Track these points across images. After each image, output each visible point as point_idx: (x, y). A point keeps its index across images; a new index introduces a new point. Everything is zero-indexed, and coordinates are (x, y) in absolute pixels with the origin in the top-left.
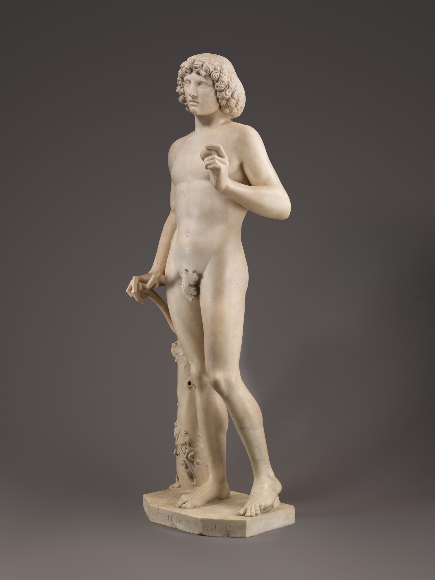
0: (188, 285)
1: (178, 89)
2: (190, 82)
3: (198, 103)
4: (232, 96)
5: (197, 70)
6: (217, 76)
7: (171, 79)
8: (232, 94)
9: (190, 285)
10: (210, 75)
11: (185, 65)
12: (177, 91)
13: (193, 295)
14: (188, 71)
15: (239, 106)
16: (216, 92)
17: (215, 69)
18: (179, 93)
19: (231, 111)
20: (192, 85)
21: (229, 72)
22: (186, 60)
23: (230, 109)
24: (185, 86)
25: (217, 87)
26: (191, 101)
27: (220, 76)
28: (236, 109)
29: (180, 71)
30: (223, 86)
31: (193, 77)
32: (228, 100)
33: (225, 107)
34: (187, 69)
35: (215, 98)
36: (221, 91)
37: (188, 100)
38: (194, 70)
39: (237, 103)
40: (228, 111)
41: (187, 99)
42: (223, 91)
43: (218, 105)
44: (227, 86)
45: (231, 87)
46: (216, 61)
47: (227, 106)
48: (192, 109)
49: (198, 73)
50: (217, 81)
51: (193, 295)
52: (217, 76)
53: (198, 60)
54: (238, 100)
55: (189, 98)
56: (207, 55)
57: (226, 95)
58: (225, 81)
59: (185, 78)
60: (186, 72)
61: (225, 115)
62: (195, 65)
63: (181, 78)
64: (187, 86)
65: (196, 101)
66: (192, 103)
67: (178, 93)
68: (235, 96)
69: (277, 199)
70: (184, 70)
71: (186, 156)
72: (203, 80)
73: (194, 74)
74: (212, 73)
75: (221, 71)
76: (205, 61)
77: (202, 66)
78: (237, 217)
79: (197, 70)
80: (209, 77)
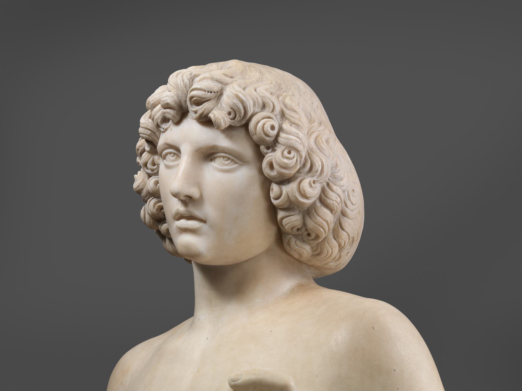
1: (140, 179)
2: (178, 150)
3: (204, 221)
4: (323, 200)
5: (201, 109)
6: (273, 128)
7: (120, 147)
8: (323, 191)
10: (246, 126)
11: (164, 94)
12: (135, 186)
14: (170, 113)
15: (344, 235)
16: (266, 183)
17: (264, 106)
19: (317, 252)
20: (185, 160)
21: (311, 121)
23: (316, 242)
24: (162, 167)
26: (179, 217)
27: (281, 129)
28: (334, 243)
29: (145, 120)
30: (292, 161)
31: (189, 134)
32: (308, 212)
33: (296, 236)
34: (167, 106)
36: (284, 181)
37: (169, 217)
38: (192, 109)
39: (340, 225)
41: (166, 210)
43: (273, 230)
44: (304, 165)
45: (318, 166)
46: (260, 80)
47: (305, 234)
48: (184, 241)
49: (206, 121)
50: (273, 145)
52: (273, 128)
53: (207, 75)
54: (343, 214)
55: (174, 206)
56: (234, 65)
58: (300, 147)
59: (161, 143)
60: (165, 120)
61: (296, 265)
62: (194, 93)
63: (148, 141)
64: (168, 167)
65: (197, 213)
66: (183, 223)
68: (333, 198)
70: (158, 112)
72: (223, 142)
75: (283, 115)
76: (228, 80)
77: (219, 95)
79: (201, 109)
80: (241, 133)
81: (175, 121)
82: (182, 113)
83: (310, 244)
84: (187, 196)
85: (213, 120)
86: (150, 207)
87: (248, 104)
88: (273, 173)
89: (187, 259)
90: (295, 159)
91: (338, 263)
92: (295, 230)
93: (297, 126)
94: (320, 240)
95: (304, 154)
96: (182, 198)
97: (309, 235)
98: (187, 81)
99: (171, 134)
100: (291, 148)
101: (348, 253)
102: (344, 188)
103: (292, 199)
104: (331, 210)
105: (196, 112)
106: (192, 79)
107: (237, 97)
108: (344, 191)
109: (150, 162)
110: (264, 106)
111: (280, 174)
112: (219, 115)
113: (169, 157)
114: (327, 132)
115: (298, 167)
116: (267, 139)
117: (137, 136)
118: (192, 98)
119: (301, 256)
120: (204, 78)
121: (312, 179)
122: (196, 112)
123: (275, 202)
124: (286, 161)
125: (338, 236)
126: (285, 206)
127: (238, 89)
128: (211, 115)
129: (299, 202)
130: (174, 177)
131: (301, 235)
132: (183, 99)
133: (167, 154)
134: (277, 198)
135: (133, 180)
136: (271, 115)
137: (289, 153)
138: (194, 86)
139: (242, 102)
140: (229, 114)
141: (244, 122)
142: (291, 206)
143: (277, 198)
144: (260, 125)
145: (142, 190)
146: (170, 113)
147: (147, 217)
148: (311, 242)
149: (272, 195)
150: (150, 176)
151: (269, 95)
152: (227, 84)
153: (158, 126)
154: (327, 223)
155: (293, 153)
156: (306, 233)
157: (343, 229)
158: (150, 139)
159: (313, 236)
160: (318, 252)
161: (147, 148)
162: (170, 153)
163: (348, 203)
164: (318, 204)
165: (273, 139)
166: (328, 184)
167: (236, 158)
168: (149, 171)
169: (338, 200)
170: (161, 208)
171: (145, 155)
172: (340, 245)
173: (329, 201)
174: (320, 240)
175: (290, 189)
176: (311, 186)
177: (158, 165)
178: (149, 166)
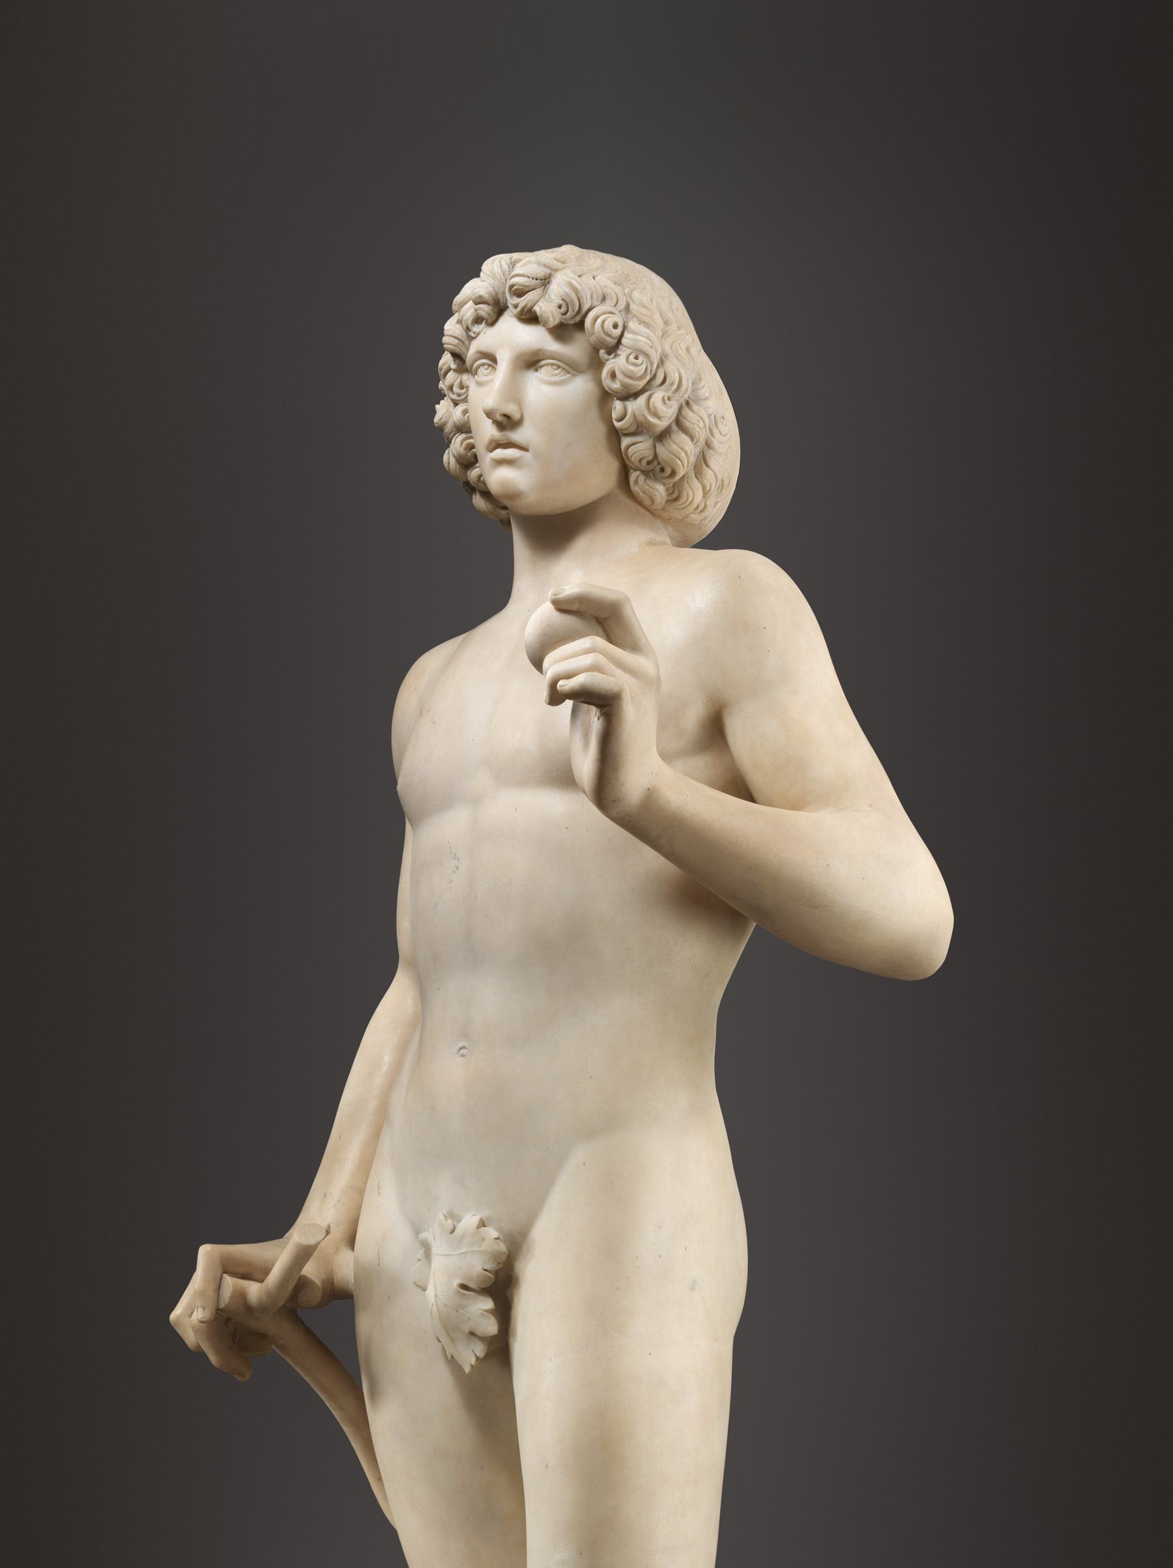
0: (456, 1282)
1: (444, 411)
3: (524, 449)
5: (523, 301)
7: (415, 364)
9: (464, 1287)
12: (436, 420)
13: (482, 1339)
15: (709, 474)
18: (448, 429)
19: (675, 495)
22: (478, 276)
25: (613, 376)
26: (496, 445)
27: (625, 328)
28: (696, 484)
29: (451, 327)
31: (511, 336)
34: (479, 301)
35: (600, 430)
36: (629, 395)
38: (512, 301)
40: (660, 491)
42: (636, 395)
45: (674, 377)
47: (656, 469)
48: (499, 478)
49: (530, 317)
50: (613, 349)
51: (482, 1339)
52: (615, 326)
54: (708, 445)
56: (568, 251)
57: (656, 415)
58: (647, 349)
64: (479, 384)
66: (500, 453)
67: (441, 428)
69: (893, 887)
71: (473, 715)
72: (552, 345)
73: (509, 324)
74: (591, 315)
75: (627, 308)
78: (704, 964)
79: (523, 301)
81: (490, 321)
82: (499, 309)
83: (664, 484)
84: (505, 415)
85: (539, 314)
86: (458, 444)
87: (583, 294)
88: (616, 386)
89: (503, 509)
90: (644, 366)
91: (703, 515)
92: (644, 462)
93: (647, 325)
94: (677, 478)
95: (702, 443)
96: (499, 418)
97: (662, 470)
98: (505, 266)
99: (487, 338)
100: (638, 353)
101: (716, 503)
102: (710, 411)
103: (640, 418)
104: (692, 439)
105: (516, 307)
106: (513, 264)
107: (570, 285)
108: (709, 416)
109: (456, 383)
110: (604, 299)
111: (624, 386)
112: (547, 307)
113: (482, 370)
114: (688, 338)
115: (648, 378)
116: (608, 339)
117: (441, 350)
118: (511, 287)
119: (653, 502)
120: (529, 262)
121: (667, 395)
122: (516, 307)
123: (617, 425)
124: (631, 367)
125: (701, 475)
126: (632, 430)
127: (571, 275)
128: (537, 308)
129: (649, 422)
130: (486, 392)
131: (653, 470)
132: (501, 290)
133: (479, 367)
134: (620, 420)
135: (435, 412)
136: (614, 310)
137: (636, 358)
138: (515, 272)
139: (576, 291)
140: (560, 307)
141: (578, 319)
142: (640, 428)
143: (620, 420)
144: (599, 321)
145: (445, 424)
146: (484, 310)
147: (452, 460)
148: (666, 481)
149: (614, 416)
150: (456, 404)
151: (612, 285)
152: (556, 270)
153: (468, 329)
154: (686, 453)
155: (641, 358)
156: (658, 468)
157: (707, 466)
158: (458, 351)
159: (668, 471)
160: (675, 495)
161: (453, 366)
162: (483, 365)
163: (715, 431)
164: (674, 427)
165: (615, 341)
166: (687, 403)
167: (571, 368)
168: (454, 397)
169: (701, 424)
170: (471, 447)
171: (451, 376)
172: (704, 488)
173: (688, 424)
174: (677, 478)
175: (636, 406)
176: (664, 403)
177: (468, 387)
178: (455, 389)
